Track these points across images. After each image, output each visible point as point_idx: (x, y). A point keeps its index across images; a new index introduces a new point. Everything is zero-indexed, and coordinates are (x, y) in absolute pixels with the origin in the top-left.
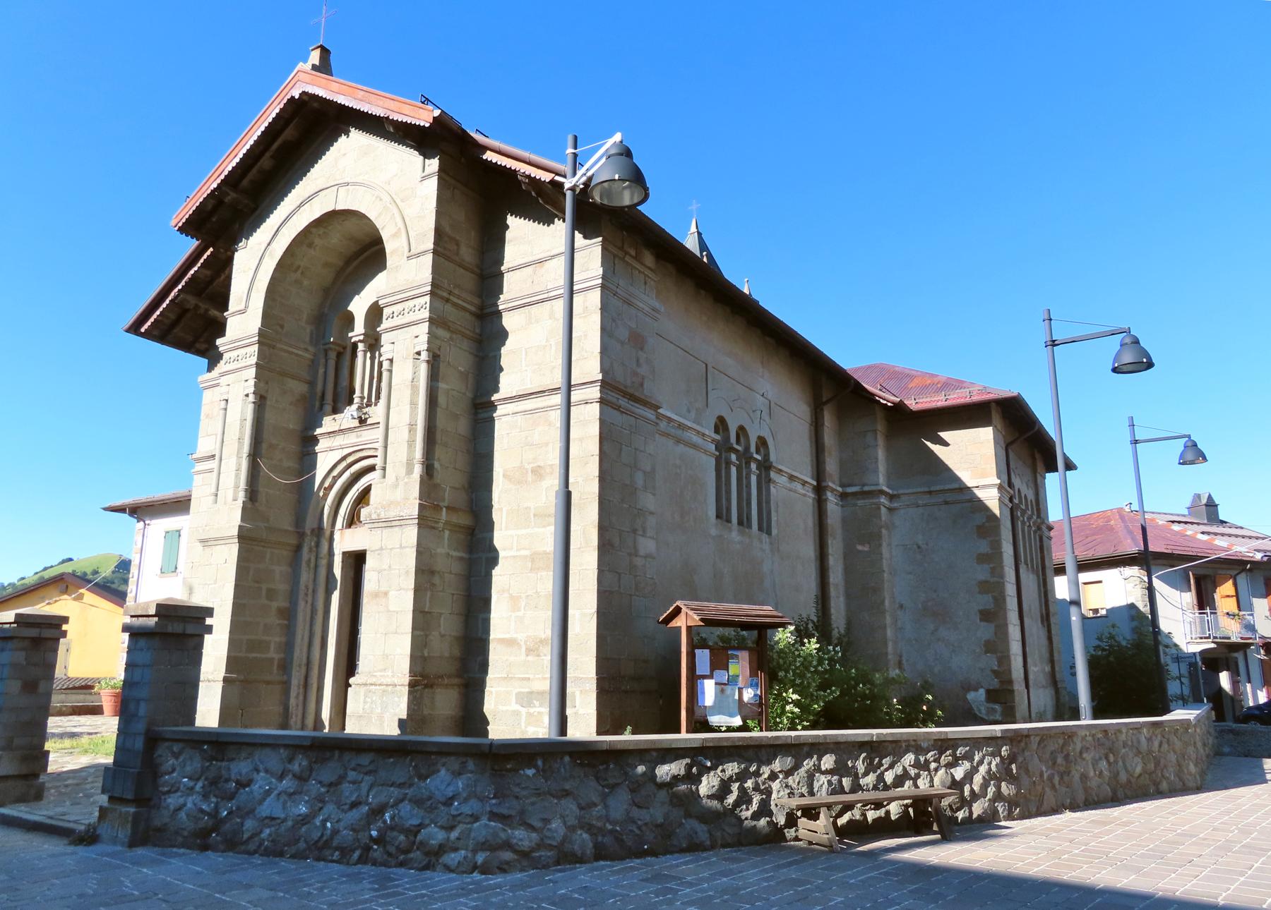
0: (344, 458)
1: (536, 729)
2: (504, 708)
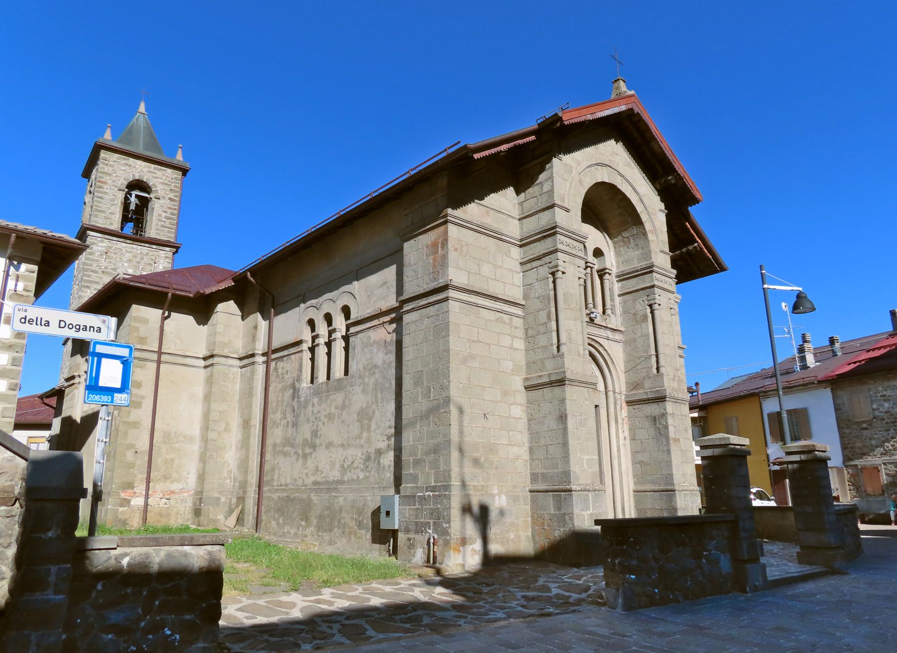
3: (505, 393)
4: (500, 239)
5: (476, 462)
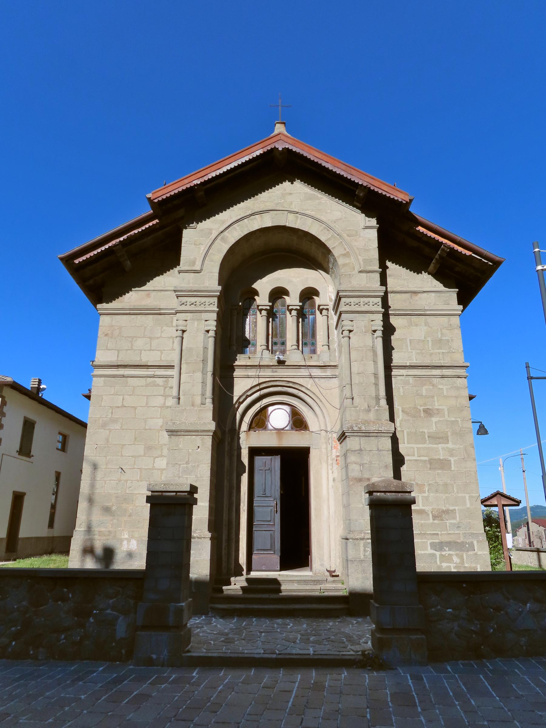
0: (259, 384)
1: (448, 564)
2: (423, 552)
3: (149, 448)
4: (160, 314)
5: (107, 510)
